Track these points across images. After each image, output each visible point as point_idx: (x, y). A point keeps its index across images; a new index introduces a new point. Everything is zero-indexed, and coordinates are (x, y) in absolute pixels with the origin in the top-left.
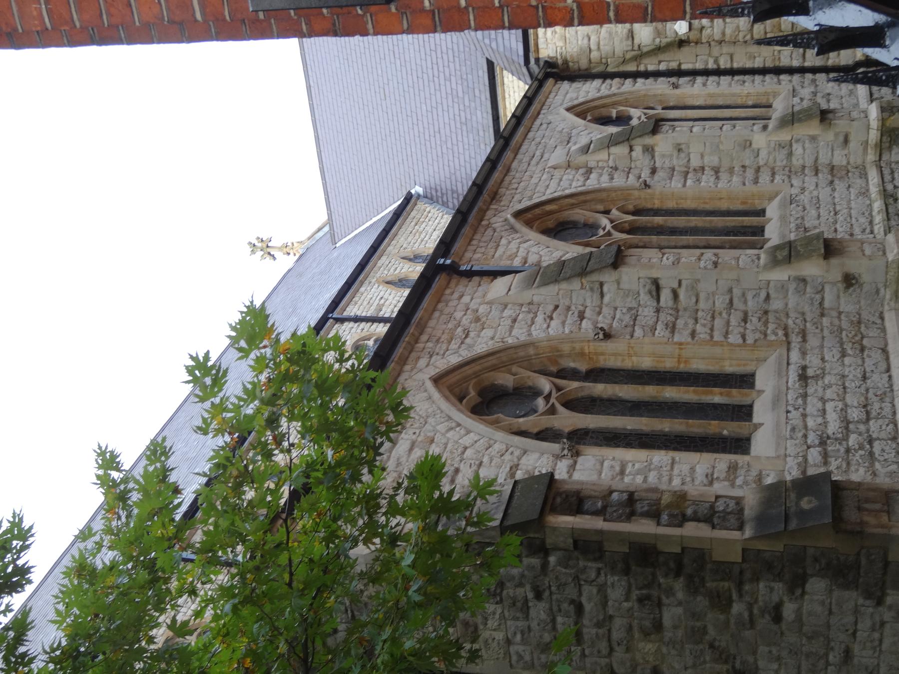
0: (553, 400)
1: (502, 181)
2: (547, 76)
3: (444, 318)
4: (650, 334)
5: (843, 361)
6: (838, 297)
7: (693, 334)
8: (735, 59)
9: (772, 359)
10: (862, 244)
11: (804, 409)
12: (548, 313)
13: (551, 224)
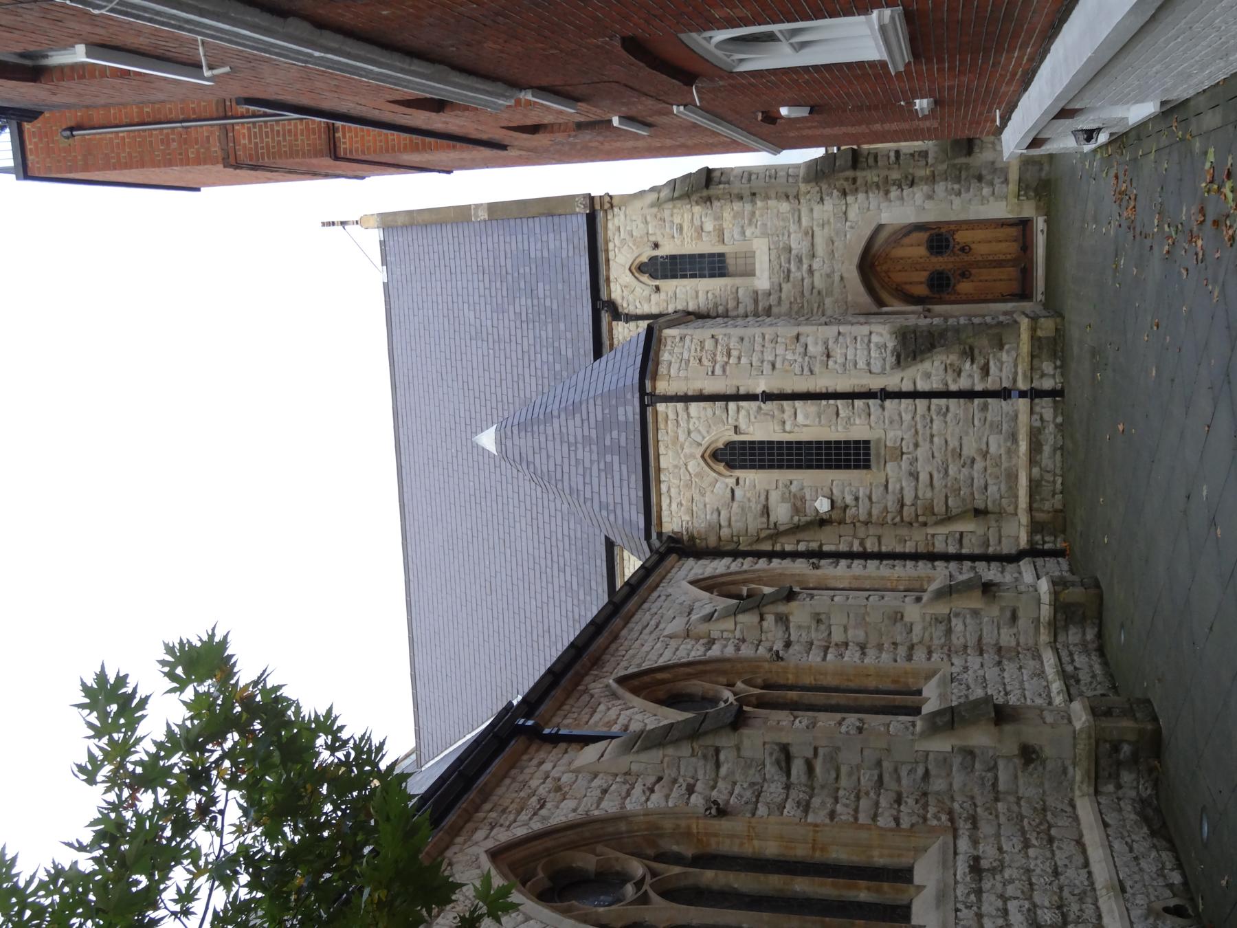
0: (646, 887)
1: (607, 647)
2: (670, 551)
3: (516, 785)
4: (777, 813)
5: (1026, 853)
6: (1016, 777)
7: (832, 815)
8: (883, 541)
9: (934, 849)
10: (1042, 711)
11: (979, 908)
12: (649, 785)
13: (661, 694)
